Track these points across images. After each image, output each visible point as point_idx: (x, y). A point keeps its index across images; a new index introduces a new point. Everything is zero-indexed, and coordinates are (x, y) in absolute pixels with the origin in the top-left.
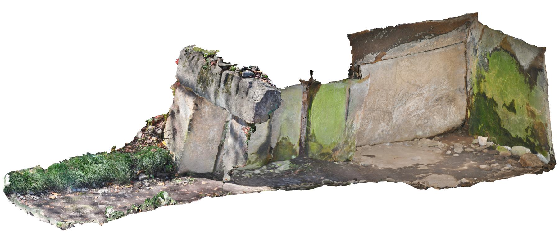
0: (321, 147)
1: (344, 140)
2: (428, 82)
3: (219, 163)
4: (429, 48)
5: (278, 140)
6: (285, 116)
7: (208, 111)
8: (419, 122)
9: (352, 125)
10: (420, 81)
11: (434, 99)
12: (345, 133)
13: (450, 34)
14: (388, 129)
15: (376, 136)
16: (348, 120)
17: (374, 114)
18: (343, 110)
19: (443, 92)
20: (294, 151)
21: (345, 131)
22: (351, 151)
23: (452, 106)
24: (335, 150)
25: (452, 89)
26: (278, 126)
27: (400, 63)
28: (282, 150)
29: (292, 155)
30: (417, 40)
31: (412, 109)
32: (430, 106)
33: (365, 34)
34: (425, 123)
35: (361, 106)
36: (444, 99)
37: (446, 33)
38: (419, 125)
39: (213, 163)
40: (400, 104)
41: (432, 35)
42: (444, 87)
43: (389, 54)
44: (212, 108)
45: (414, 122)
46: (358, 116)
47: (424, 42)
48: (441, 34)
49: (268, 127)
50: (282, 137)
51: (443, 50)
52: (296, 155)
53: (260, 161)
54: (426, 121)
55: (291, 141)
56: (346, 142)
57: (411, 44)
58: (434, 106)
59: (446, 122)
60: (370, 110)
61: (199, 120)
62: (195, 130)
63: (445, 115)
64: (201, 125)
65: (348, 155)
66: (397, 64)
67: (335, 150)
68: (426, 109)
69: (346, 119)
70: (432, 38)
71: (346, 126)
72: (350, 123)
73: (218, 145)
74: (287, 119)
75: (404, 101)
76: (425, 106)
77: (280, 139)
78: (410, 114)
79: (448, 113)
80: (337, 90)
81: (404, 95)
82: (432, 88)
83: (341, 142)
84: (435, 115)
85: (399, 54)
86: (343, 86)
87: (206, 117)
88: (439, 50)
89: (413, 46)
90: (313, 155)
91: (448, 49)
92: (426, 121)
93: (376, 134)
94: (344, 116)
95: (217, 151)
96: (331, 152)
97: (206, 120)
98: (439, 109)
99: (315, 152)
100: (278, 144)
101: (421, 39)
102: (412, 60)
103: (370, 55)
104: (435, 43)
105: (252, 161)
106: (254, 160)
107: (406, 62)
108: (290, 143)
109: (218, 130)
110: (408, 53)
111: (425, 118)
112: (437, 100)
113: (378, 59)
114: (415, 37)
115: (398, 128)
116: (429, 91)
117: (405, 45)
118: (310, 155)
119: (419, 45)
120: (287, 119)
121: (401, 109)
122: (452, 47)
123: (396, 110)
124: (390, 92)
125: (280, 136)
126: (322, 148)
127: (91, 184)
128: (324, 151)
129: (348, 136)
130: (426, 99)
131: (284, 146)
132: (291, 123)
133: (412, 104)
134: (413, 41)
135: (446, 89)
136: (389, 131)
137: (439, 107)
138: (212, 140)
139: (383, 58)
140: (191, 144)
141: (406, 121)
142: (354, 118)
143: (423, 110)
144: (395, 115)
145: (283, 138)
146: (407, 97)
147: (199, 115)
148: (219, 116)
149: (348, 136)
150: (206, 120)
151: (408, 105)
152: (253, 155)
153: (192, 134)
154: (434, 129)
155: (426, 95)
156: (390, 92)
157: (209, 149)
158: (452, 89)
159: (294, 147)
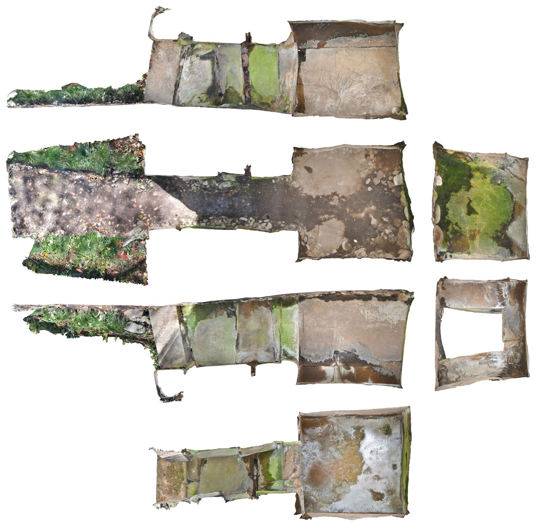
0: (261, 97)
1: (280, 95)
2: (366, 72)
3: (176, 99)
4: (365, 45)
5: (226, 87)
6: (228, 68)
7: (163, 55)
8: (363, 104)
9: (284, 83)
10: (359, 69)
11: (373, 86)
12: (279, 89)
13: (382, 36)
14: (337, 106)
15: (326, 110)
16: (281, 78)
17: (321, 89)
18: (275, 70)
19: (379, 82)
20: (240, 99)
21: (279, 87)
22: (287, 104)
23: (388, 95)
24: (273, 102)
25: (386, 81)
26: (225, 76)
27: (339, 52)
28: (230, 96)
29: (239, 102)
30: (353, 36)
31: (355, 92)
32: (370, 92)
33: (527, 164)
34: (367, 106)
35: (290, 68)
36: (380, 88)
37: (377, 35)
38: (363, 107)
39: (172, 98)
40: (345, 87)
41: (366, 35)
42: (380, 78)
43: (329, 43)
44: (166, 53)
45: (359, 103)
46: (289, 76)
47: (358, 39)
48: (373, 35)
49: (212, 73)
50: (228, 86)
51: (377, 48)
52: (242, 102)
53: (211, 101)
54: (368, 104)
55: (237, 90)
56: (282, 97)
57: (348, 38)
58: (373, 92)
59: (385, 107)
60: (317, 86)
61: (156, 60)
62: (154, 68)
63: (384, 102)
64: (158, 66)
65: (285, 108)
66: (337, 52)
67: (273, 102)
68: (367, 94)
69: (279, 77)
70: (366, 37)
71: (280, 84)
72: (283, 81)
73: (174, 84)
74: (231, 71)
75: (348, 85)
76: (365, 91)
77: (228, 87)
78: (354, 97)
79: (386, 100)
80: (268, 52)
81: (346, 80)
82: (370, 77)
83: (278, 96)
84: (375, 101)
85: (337, 44)
86: (274, 51)
87: (162, 59)
88: (373, 48)
89: (349, 41)
90: (255, 103)
91: (381, 49)
92: (368, 104)
93: (326, 107)
94: (277, 75)
95: (174, 88)
96: (269, 102)
97: (162, 61)
98: (378, 96)
99: (256, 100)
100: (226, 91)
101: (356, 36)
102: (349, 52)
103: (312, 41)
104: (369, 42)
105: (203, 100)
106: (205, 99)
107: (344, 52)
108: (236, 92)
109: (173, 71)
110: (346, 45)
111: (368, 102)
112: (375, 88)
113: (320, 46)
114: (351, 34)
115: (347, 107)
116: (367, 79)
117: (342, 38)
118: (252, 103)
119: (355, 40)
120: (231, 71)
121: (346, 91)
122: (385, 48)
123: (342, 91)
124: (333, 74)
125: (227, 84)
126: (262, 98)
127: (74, 101)
128: (264, 101)
129: (283, 92)
130: (366, 86)
131: (231, 93)
132: (234, 75)
133: (356, 88)
134: (349, 36)
135: (381, 80)
136: (338, 107)
137: (377, 94)
138: (169, 79)
139: (325, 46)
140: (153, 80)
141: (352, 102)
142: (285, 77)
143: (365, 95)
144: (342, 95)
145: (230, 87)
146: (348, 82)
147: (156, 57)
148: (172, 60)
149: (283, 92)
150: (162, 61)
151: (351, 89)
152: (203, 95)
153: (152, 70)
154: (376, 111)
155: (365, 82)
156: (333, 74)
157: (167, 86)
158: (386, 81)
159: (240, 96)
